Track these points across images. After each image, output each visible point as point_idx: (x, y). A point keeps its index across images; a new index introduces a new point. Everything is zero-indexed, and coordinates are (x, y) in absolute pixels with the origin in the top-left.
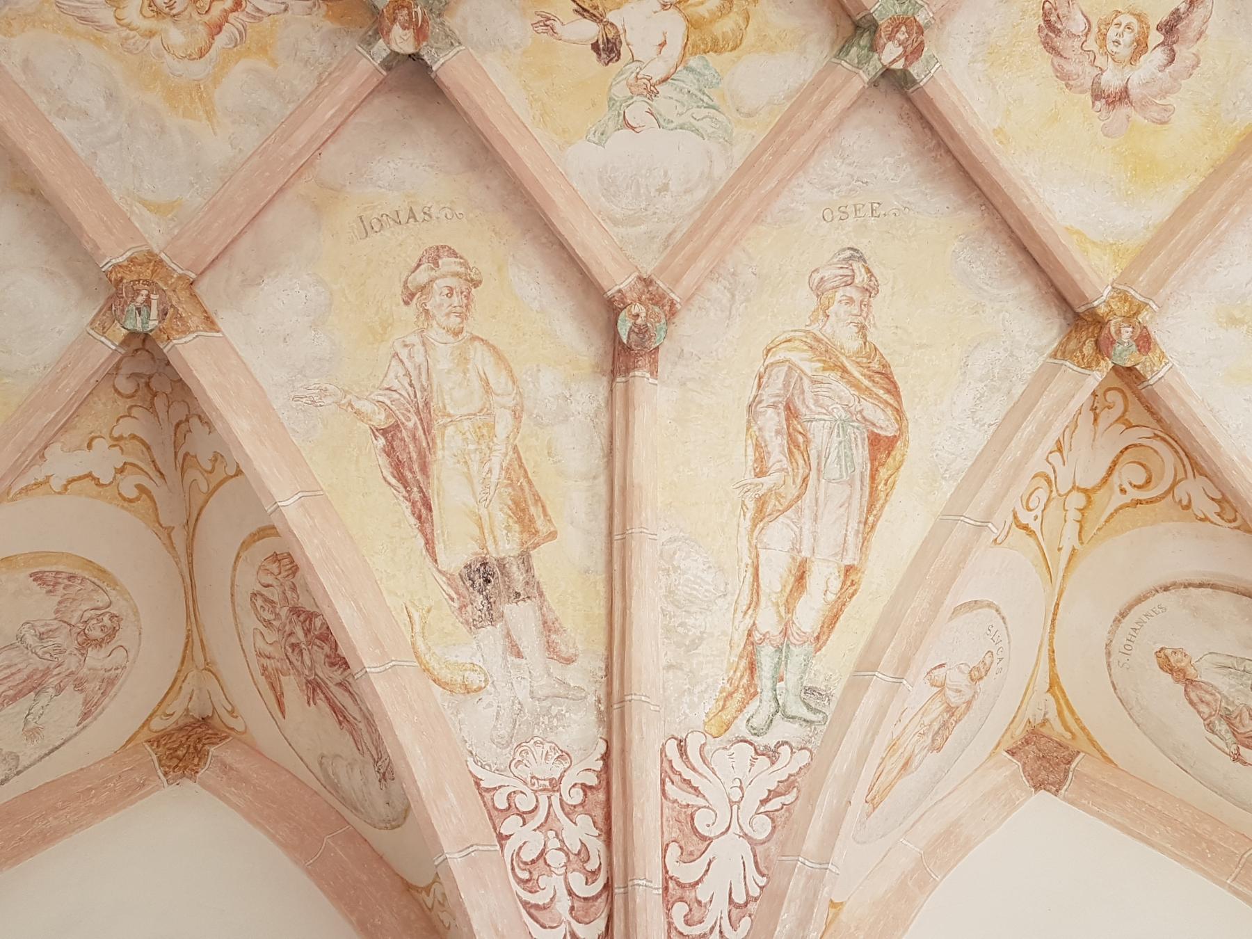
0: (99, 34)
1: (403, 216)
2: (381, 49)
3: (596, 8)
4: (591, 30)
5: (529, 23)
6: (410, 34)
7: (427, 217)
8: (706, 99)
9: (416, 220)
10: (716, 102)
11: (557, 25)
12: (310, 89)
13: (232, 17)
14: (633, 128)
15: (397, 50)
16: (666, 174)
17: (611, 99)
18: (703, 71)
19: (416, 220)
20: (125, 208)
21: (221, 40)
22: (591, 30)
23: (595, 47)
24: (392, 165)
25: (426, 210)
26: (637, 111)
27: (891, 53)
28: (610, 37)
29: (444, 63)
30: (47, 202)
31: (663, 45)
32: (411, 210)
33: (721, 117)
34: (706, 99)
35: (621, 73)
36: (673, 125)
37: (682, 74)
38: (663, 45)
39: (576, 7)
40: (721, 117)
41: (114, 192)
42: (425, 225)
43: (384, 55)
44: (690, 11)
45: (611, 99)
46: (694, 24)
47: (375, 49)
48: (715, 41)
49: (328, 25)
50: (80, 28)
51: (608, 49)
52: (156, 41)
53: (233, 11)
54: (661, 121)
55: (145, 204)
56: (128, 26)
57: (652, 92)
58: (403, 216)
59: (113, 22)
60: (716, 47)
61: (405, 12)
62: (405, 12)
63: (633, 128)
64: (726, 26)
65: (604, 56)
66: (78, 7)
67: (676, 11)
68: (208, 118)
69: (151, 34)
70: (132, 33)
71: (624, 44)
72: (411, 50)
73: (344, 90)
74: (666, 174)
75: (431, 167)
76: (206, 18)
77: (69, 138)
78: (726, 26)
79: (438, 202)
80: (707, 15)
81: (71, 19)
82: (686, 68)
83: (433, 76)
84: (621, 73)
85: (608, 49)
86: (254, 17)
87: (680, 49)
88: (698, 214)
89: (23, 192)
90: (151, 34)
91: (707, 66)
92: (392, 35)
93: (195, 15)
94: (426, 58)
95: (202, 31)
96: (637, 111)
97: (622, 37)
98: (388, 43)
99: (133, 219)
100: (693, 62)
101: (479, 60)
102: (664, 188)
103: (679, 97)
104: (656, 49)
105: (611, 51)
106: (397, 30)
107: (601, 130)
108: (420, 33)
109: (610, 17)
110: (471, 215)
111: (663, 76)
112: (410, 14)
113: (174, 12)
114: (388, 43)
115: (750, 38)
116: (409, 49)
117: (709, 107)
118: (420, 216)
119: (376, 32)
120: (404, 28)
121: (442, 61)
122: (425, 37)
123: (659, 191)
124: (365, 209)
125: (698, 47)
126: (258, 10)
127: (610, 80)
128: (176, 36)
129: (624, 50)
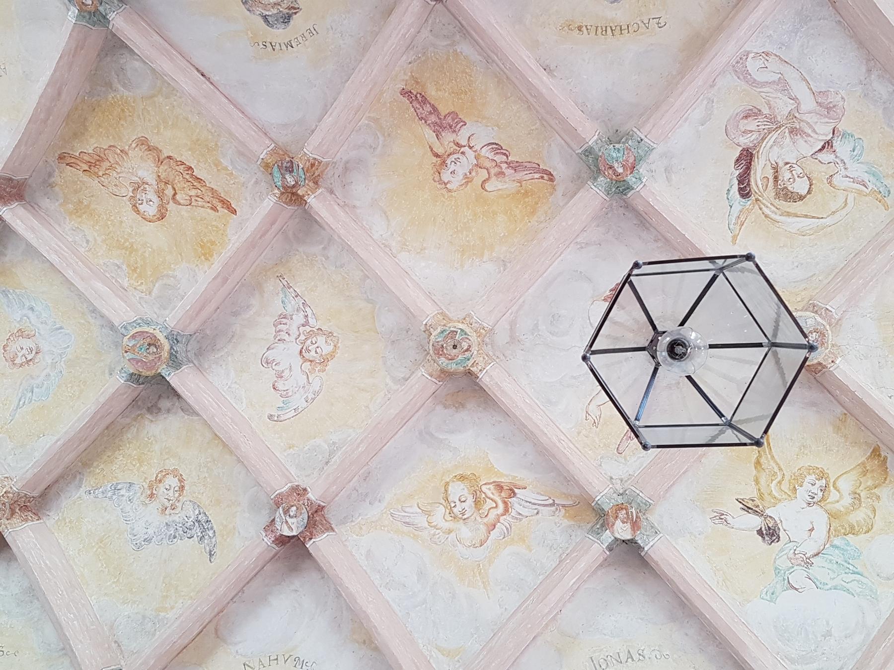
0: (416, 533)
1: (623, 657)
2: (607, 537)
3: (758, 506)
4: (756, 522)
5: (708, 517)
6: (628, 526)
7: (641, 658)
8: (851, 567)
9: (633, 660)
10: (859, 570)
11: (729, 519)
12: (554, 566)
13: (502, 518)
14: (796, 589)
15: (619, 537)
16: (828, 623)
17: (776, 568)
18: (846, 547)
19: (633, 660)
20: (426, 653)
21: (494, 534)
22: (756, 522)
23: (760, 532)
24: (613, 618)
25: (640, 652)
26: (798, 577)
27: (622, 531)
28: (770, 525)
29: (653, 546)
30: (376, 649)
31: (812, 530)
32: (629, 652)
33: (865, 580)
34: (851, 567)
35: (782, 550)
36: (829, 586)
37: (829, 550)
38: (812, 530)
39: (742, 506)
40: (865, 580)
41: (420, 641)
42: (639, 663)
43: (610, 540)
44: (828, 507)
45: (776, 568)
46: (833, 515)
47: (604, 537)
48: (852, 527)
49: (566, 522)
50: (406, 529)
51: (770, 534)
52: (453, 535)
53: (503, 515)
54: (818, 583)
55: (439, 649)
56: (435, 527)
57: (808, 564)
58: (623, 657)
59: (426, 524)
60: (852, 530)
61: (624, 511)
62: (624, 511)
63: (796, 589)
64: (859, 516)
65: (767, 538)
66: (404, 516)
67: (819, 507)
68: (485, 588)
69: (450, 531)
70: (438, 531)
71: (782, 530)
72: (629, 537)
73: (582, 565)
74: (828, 623)
75: (642, 619)
76: (485, 520)
77: (391, 603)
78: (859, 516)
79: (649, 646)
80: (842, 509)
81: (399, 524)
82: (833, 546)
83: (643, 554)
84: (782, 550)
85: (770, 534)
86: (517, 519)
87: (825, 532)
88: (859, 655)
89: (358, 642)
90: (450, 531)
91: (848, 544)
92: (615, 527)
93: (478, 518)
94: (639, 542)
95: (483, 529)
96: (798, 577)
97: (780, 526)
98: (612, 533)
99: (431, 661)
100: (837, 541)
101: (673, 543)
102: (828, 634)
103: (830, 566)
104: (808, 533)
105: (773, 535)
106: (618, 523)
107: (771, 591)
108: (635, 525)
109: (768, 512)
110: (675, 656)
111: (815, 552)
112: (627, 513)
113: (465, 517)
114: (612, 533)
115: (878, 523)
116: (628, 536)
117: (854, 573)
118: (636, 657)
119: (602, 526)
120: (623, 522)
121: (651, 544)
122: (639, 528)
123: (824, 636)
124: (594, 652)
125: (839, 531)
126: (520, 514)
127: (774, 555)
128: (465, 532)
129: (782, 534)
